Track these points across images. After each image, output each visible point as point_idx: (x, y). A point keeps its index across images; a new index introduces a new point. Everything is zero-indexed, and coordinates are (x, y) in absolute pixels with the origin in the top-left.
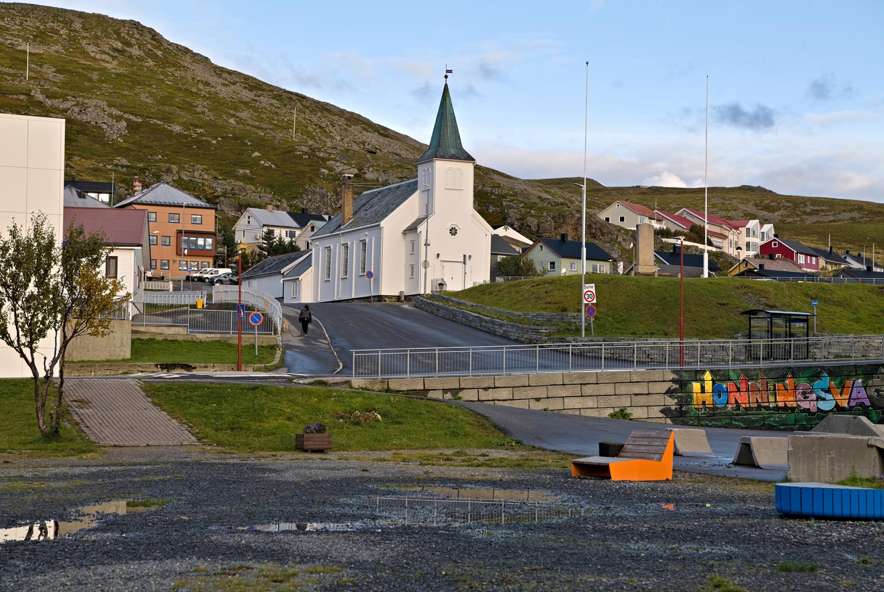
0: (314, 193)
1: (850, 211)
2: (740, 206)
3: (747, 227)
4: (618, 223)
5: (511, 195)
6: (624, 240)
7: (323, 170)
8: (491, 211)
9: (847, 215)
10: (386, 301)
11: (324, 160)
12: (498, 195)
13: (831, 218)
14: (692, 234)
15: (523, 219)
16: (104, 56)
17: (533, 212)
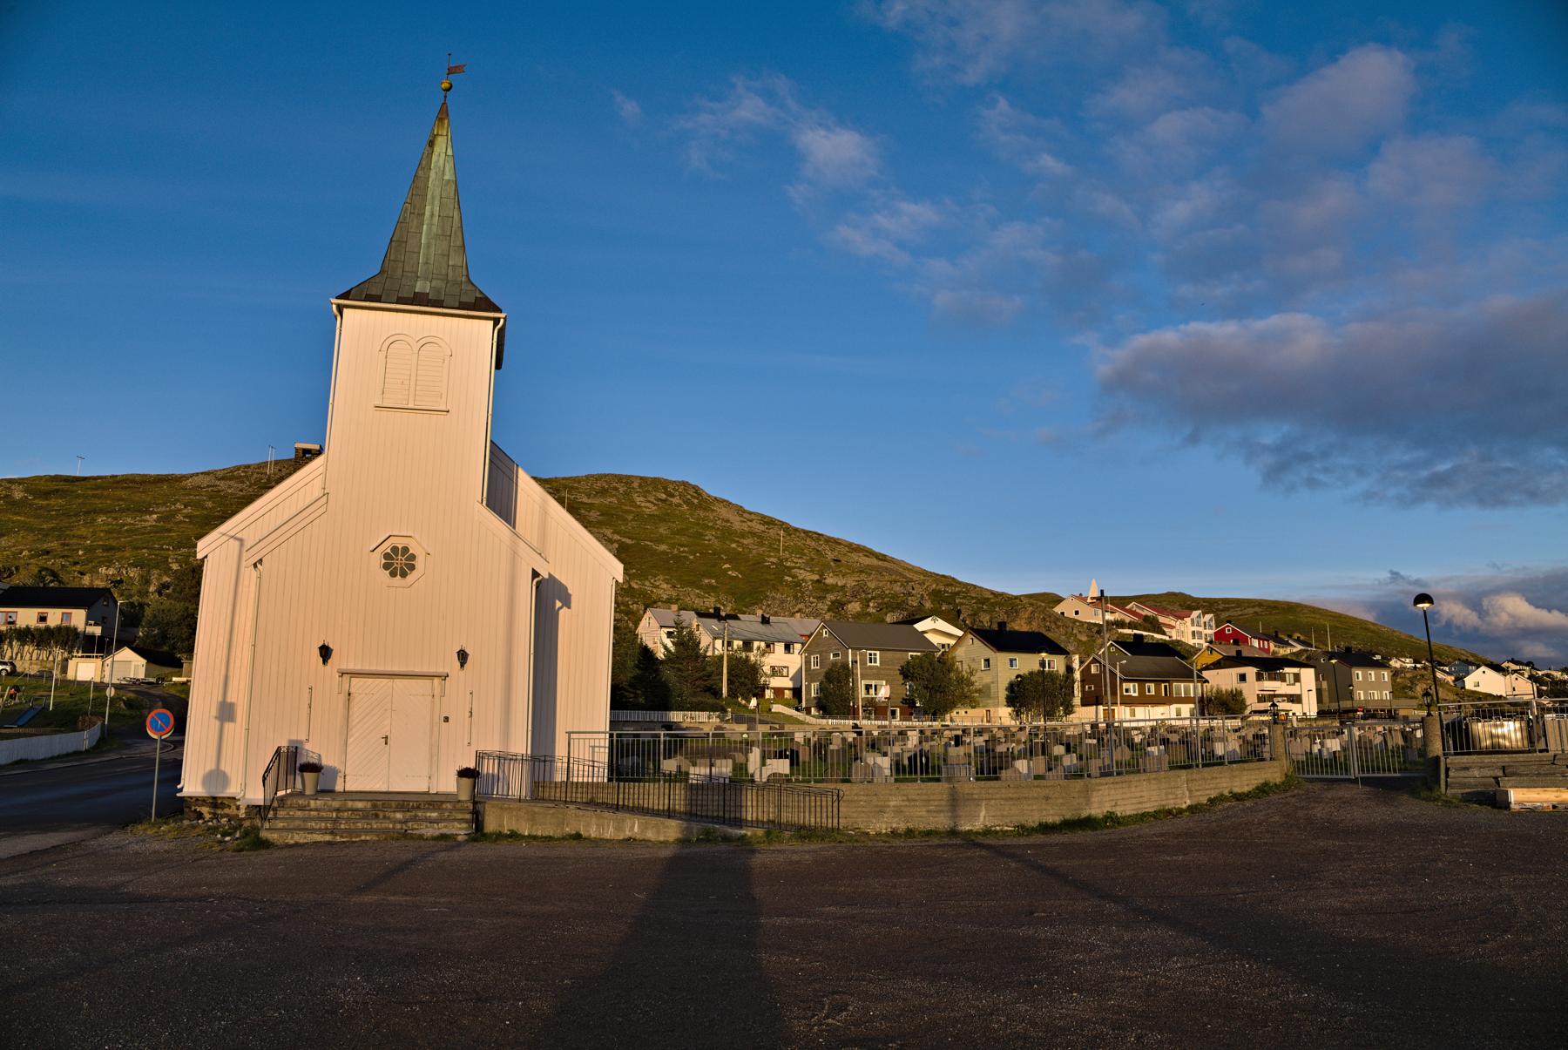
0: (774, 599)
1: (1253, 607)
2: (1168, 606)
3: (1192, 616)
4: (1074, 616)
5: (963, 592)
6: (1080, 632)
7: (787, 578)
8: (944, 608)
9: (1251, 611)
10: (200, 815)
11: (790, 568)
12: (951, 593)
13: (1240, 613)
14: (1147, 625)
15: (975, 615)
16: (648, 504)
17: (984, 607)
